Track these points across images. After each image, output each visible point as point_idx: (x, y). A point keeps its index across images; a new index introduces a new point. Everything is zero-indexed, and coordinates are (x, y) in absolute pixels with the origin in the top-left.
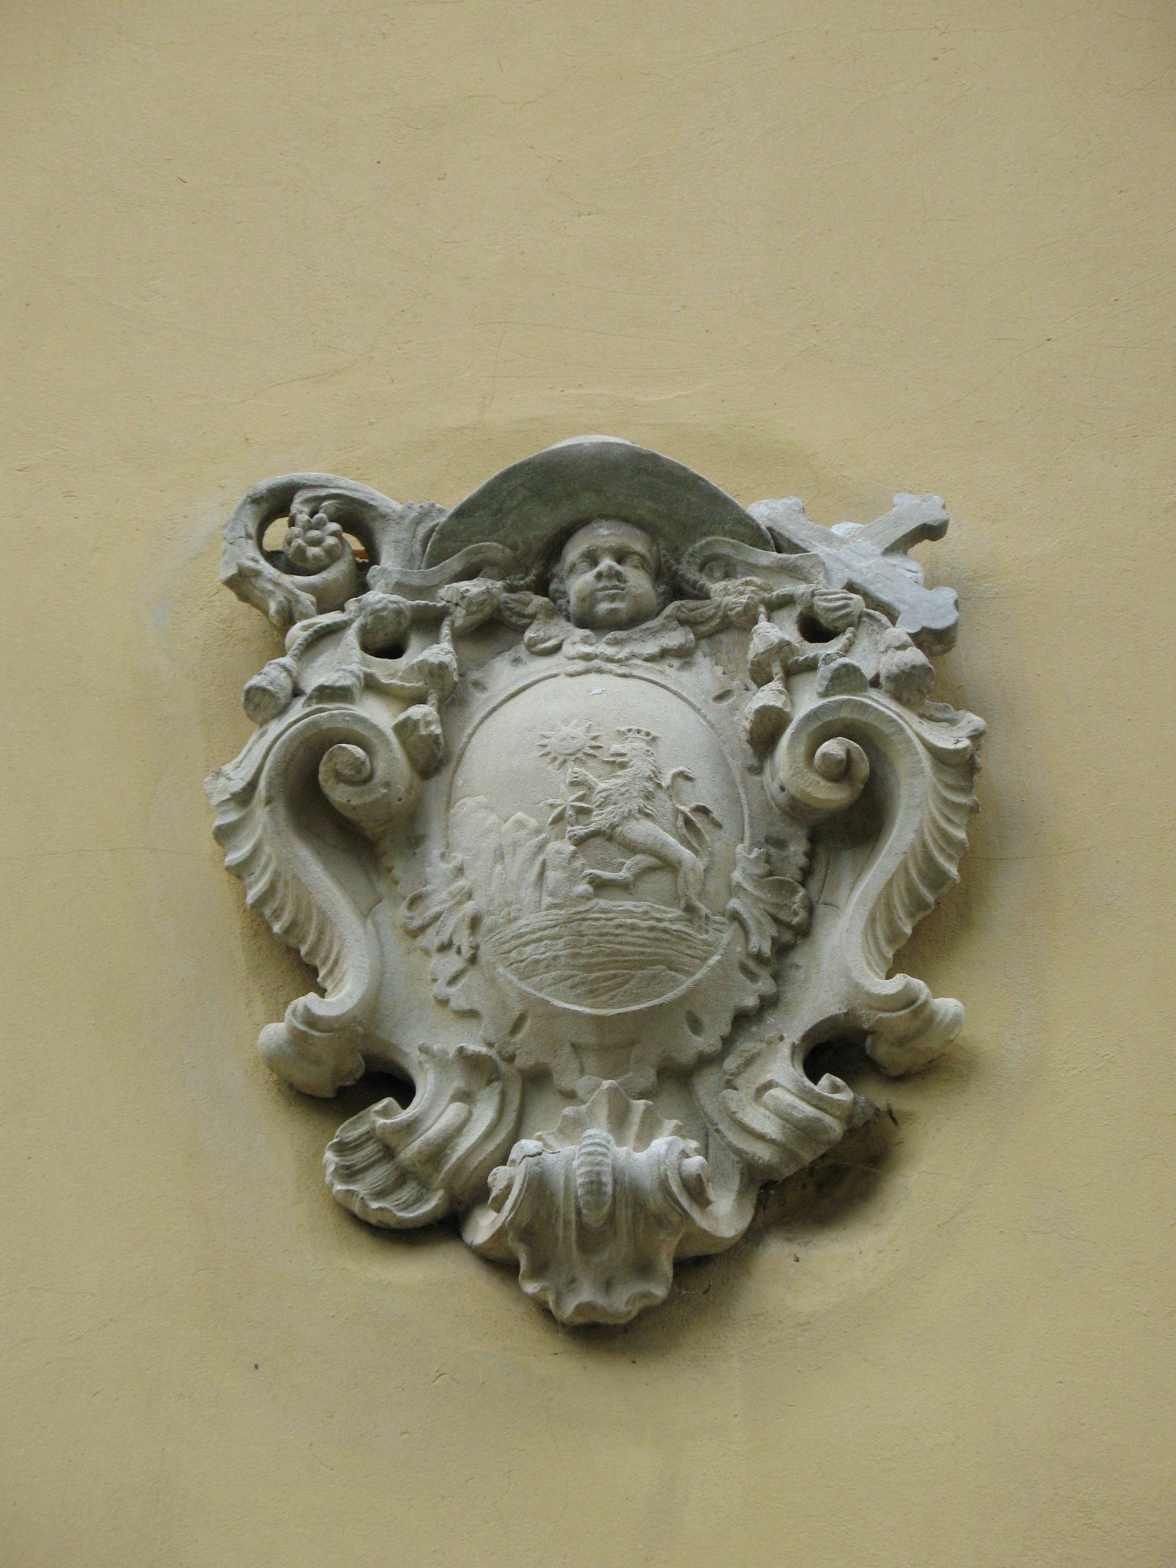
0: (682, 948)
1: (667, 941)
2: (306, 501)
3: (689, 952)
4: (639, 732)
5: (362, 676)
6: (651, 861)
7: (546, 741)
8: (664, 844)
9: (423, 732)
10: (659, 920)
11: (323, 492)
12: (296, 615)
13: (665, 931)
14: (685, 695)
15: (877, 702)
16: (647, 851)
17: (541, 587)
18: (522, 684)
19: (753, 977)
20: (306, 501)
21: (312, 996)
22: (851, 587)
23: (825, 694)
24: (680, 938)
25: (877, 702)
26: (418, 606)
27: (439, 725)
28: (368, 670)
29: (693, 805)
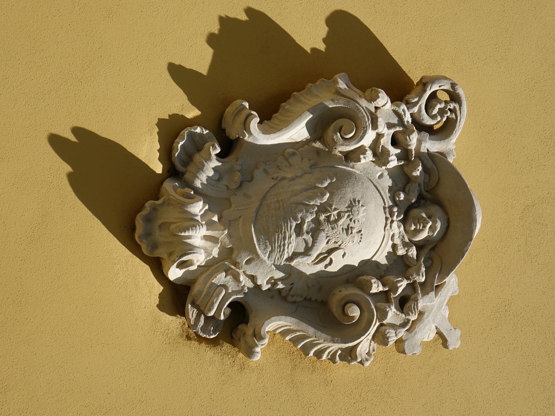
0: (278, 256)
1: (280, 251)
2: (454, 107)
3: (277, 258)
4: (361, 238)
5: (383, 133)
6: (310, 245)
7: (357, 202)
8: (317, 250)
9: (362, 156)
10: (288, 247)
11: (458, 112)
12: (408, 106)
13: (284, 250)
14: (380, 190)
15: (374, 325)
16: (313, 245)
17: (421, 197)
18: (382, 192)
19: (268, 283)
20: (454, 107)
21: (258, 119)
22: (421, 314)
23: (383, 146)
24: (281, 255)
25: (374, 325)
26: (412, 152)
27: (334, 219)
28: (385, 135)
29: (333, 259)
